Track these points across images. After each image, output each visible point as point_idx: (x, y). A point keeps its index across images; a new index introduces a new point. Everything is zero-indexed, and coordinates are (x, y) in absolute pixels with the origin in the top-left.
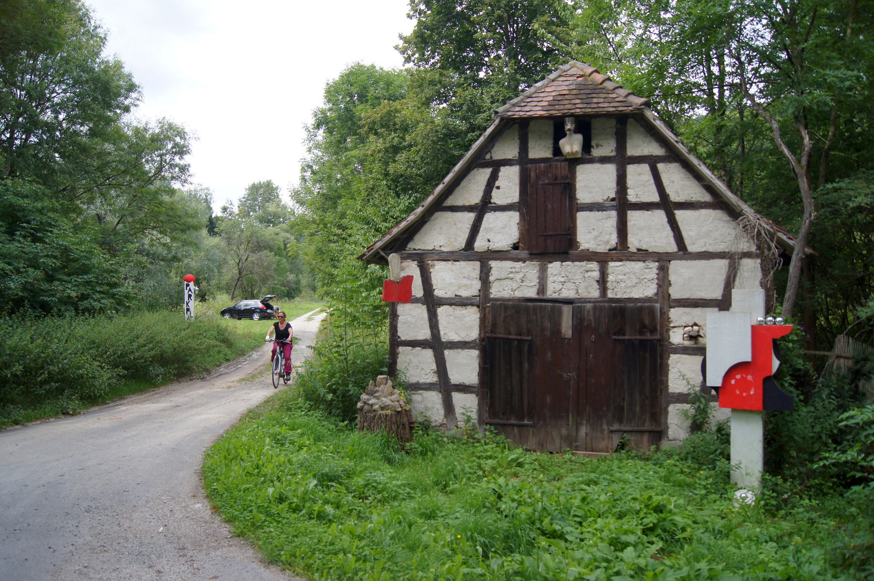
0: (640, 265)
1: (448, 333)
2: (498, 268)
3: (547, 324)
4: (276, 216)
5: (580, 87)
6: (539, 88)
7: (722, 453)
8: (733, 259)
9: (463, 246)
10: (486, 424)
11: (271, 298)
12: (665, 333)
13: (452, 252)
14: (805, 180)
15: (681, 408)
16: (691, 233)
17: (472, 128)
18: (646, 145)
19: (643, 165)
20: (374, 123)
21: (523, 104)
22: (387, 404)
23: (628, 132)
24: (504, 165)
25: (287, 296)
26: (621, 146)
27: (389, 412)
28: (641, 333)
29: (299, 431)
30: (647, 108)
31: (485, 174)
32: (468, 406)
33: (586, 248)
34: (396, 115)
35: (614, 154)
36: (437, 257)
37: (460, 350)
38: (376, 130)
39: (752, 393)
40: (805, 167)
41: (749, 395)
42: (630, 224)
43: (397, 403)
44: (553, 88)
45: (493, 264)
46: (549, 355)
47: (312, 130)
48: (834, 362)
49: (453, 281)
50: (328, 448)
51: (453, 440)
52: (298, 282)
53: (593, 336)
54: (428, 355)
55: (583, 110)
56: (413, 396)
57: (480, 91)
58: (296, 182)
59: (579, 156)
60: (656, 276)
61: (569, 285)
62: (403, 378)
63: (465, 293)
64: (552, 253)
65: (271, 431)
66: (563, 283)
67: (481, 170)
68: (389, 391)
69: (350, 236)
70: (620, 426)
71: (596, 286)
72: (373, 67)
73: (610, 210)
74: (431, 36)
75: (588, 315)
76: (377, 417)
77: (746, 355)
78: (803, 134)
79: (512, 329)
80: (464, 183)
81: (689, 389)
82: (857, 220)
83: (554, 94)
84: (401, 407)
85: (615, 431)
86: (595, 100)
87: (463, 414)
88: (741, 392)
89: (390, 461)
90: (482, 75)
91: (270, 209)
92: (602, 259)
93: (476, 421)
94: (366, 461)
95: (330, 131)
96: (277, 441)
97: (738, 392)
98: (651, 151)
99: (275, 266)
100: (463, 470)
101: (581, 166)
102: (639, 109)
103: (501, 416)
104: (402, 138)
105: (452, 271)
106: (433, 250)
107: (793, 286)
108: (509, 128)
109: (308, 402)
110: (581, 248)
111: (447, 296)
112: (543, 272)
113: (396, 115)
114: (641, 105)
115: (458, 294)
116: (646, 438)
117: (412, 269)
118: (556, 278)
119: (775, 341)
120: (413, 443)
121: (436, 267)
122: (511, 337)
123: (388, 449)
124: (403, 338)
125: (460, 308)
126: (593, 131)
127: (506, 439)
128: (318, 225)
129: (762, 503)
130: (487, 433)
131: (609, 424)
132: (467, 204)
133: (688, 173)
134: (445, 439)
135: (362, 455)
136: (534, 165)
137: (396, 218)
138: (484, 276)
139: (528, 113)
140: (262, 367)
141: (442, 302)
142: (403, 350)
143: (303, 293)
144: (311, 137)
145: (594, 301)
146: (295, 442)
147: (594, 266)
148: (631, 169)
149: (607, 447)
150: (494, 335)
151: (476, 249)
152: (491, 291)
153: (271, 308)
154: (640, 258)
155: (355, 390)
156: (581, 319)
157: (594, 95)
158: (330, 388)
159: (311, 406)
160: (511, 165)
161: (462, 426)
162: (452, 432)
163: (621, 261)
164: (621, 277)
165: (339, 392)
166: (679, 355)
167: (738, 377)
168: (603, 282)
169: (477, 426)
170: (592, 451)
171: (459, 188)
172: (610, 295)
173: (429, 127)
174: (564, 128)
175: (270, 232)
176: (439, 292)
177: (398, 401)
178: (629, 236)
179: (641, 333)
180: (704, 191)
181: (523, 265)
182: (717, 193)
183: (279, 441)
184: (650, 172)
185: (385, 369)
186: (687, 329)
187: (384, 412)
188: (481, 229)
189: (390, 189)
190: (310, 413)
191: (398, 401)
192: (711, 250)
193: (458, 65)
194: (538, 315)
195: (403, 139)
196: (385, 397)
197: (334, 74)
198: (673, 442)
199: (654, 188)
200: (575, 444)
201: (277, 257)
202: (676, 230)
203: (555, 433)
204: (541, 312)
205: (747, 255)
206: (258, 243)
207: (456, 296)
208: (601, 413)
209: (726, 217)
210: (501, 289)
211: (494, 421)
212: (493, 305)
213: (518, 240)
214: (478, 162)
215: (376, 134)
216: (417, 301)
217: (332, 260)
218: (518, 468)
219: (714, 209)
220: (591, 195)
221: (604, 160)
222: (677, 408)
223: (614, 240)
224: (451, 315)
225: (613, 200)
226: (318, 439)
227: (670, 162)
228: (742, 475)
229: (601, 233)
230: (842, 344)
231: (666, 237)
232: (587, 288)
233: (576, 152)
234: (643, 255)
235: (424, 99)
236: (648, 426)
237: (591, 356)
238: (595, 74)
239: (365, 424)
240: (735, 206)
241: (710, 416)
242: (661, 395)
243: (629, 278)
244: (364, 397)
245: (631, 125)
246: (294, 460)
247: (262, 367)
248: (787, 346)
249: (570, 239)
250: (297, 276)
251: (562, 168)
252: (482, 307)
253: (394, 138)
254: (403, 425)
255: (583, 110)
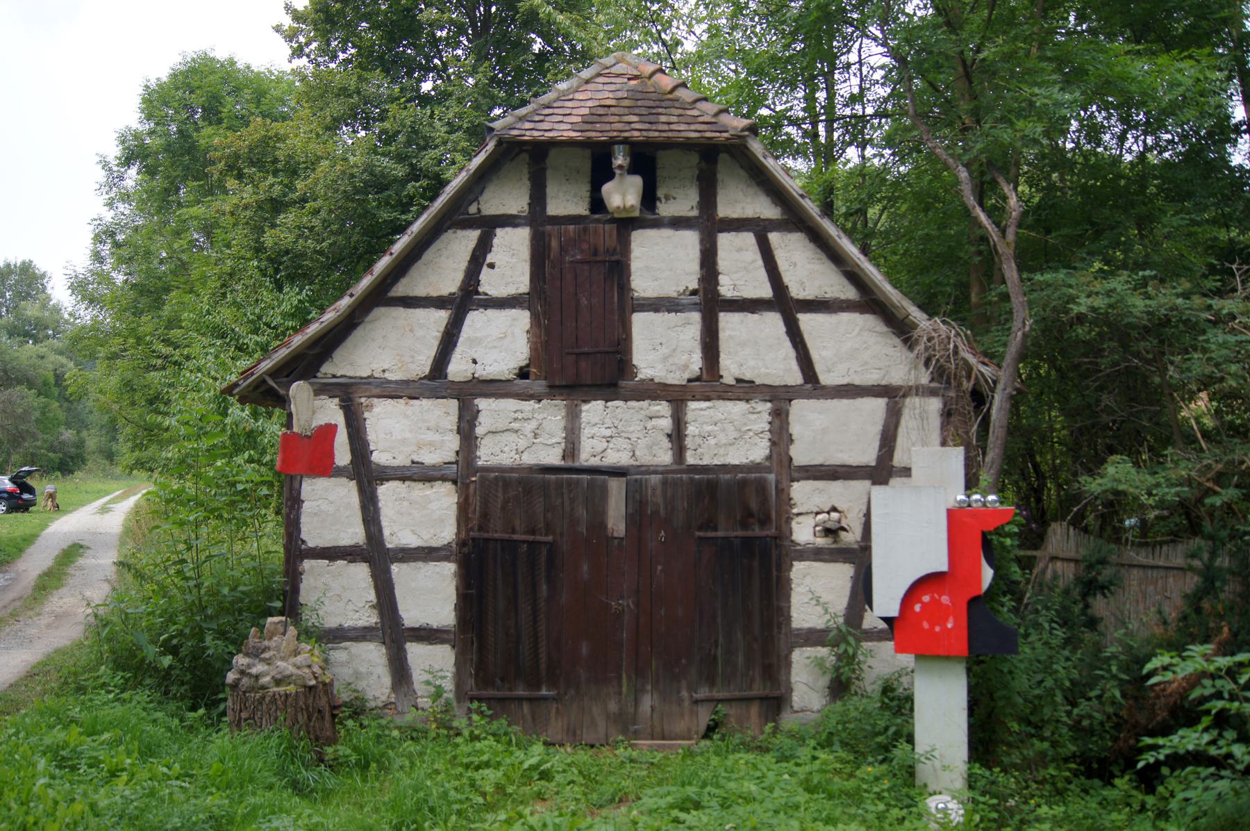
0: (741, 407)
1: (397, 533)
2: (490, 410)
3: (582, 512)
4: (41, 325)
5: (636, 95)
6: (565, 93)
7: (898, 735)
8: (892, 395)
9: (427, 370)
10: (472, 700)
11: (29, 473)
12: (784, 525)
13: (406, 383)
14: (1013, 265)
15: (813, 655)
16: (824, 353)
17: (415, 174)
18: (749, 200)
19: (745, 234)
20: (237, 156)
21: (537, 118)
22: (288, 673)
23: (719, 177)
24: (503, 226)
25: (59, 469)
26: (708, 200)
27: (291, 689)
28: (745, 525)
29: (106, 736)
30: (753, 136)
31: (466, 240)
32: (437, 667)
33: (649, 376)
34: (278, 145)
35: (695, 213)
36: (377, 391)
37: (420, 564)
38: (240, 170)
39: (950, 626)
40: (1013, 245)
41: (945, 629)
42: (723, 335)
43: (307, 670)
44: (588, 95)
45: (482, 404)
46: (585, 568)
47: (115, 169)
48: (1047, 567)
49: (408, 435)
50: (169, 768)
51: (414, 733)
52: (80, 444)
53: (663, 533)
54: (361, 573)
55: (645, 134)
56: (332, 652)
57: (429, 112)
58: (82, 262)
59: (637, 214)
60: (767, 427)
61: (620, 442)
62: (314, 620)
63: (430, 458)
64: (588, 386)
65: (48, 741)
66: (609, 439)
67: (460, 233)
68: (292, 648)
69: (188, 358)
70: (711, 691)
71: (666, 444)
72: (232, 63)
73: (690, 310)
74: (341, 13)
75: (654, 494)
76: (267, 699)
77: (939, 562)
78: (1006, 190)
79: (517, 523)
80: (428, 255)
81: (829, 621)
82: (1077, 336)
83: (590, 104)
84: (316, 678)
85: (702, 701)
86: (663, 119)
87: (428, 683)
88: (932, 625)
89: (298, 788)
90: (426, 87)
91: (29, 313)
92: (677, 396)
93: (451, 696)
94: (254, 794)
95: (150, 171)
96: (62, 763)
97: (926, 625)
98: (758, 210)
99: (37, 414)
100: (445, 794)
101: (640, 231)
102: (740, 137)
103: (498, 681)
104: (286, 186)
105: (406, 416)
106: (369, 377)
107: (999, 442)
108: (512, 160)
109: (121, 674)
110: (640, 376)
111: (396, 463)
112: (573, 418)
113: (278, 145)
114: (743, 130)
115: (416, 459)
116: (754, 710)
117: (330, 412)
118: (595, 430)
119: (984, 535)
120: (339, 747)
121: (376, 410)
122: (515, 537)
123: (293, 763)
124: (311, 544)
125: (420, 485)
126: (659, 173)
127: (509, 725)
128: (126, 338)
129: (977, 818)
130: (475, 717)
131: (692, 689)
132: (434, 294)
133: (819, 251)
134: (396, 733)
135: (237, 784)
136: (556, 227)
137: (274, 328)
138: (465, 425)
139: (547, 134)
140: (18, 603)
141: (387, 474)
142: (312, 567)
143: (90, 464)
144: (114, 179)
145: (664, 471)
146: (100, 762)
147: (663, 408)
148: (725, 241)
149: (689, 730)
150: (486, 535)
151: (450, 378)
152: (478, 454)
153: (31, 490)
154: (742, 396)
155: (216, 647)
156: (641, 502)
157: (660, 110)
158: (165, 644)
159: (127, 680)
160: (515, 226)
161: (426, 706)
162: (408, 718)
163: (708, 399)
164: (710, 428)
165: (183, 652)
166: (807, 563)
167: (926, 599)
168: (677, 437)
169: (455, 704)
170: (663, 739)
171: (419, 264)
172: (691, 459)
173: (338, 167)
174: (611, 163)
175: (29, 354)
176: (380, 457)
177: (309, 666)
178: (723, 357)
179: (745, 525)
180: (845, 282)
181: (537, 406)
182: (867, 285)
183: (65, 761)
184: (757, 247)
185: (278, 604)
186: (820, 517)
187: (281, 689)
188: (461, 340)
189: (265, 275)
190: (125, 695)
191: (309, 666)
192: (857, 382)
193: (390, 65)
194: (566, 497)
195: (291, 187)
196: (282, 659)
197: (160, 70)
198: (801, 715)
199: (762, 274)
200: (632, 728)
201: (42, 399)
202: (800, 346)
203: (596, 711)
204: (570, 491)
205: (918, 390)
206: (5, 371)
207: (413, 462)
208: (677, 670)
209: (880, 327)
210: (497, 450)
211: (484, 693)
212: (483, 479)
213: (527, 362)
214: (454, 218)
215: (240, 176)
216: (339, 472)
217: (151, 402)
218: (543, 782)
219: (862, 313)
220: (656, 283)
221: (678, 223)
222: (807, 654)
223: (696, 363)
224: (403, 499)
225: (694, 293)
226: (148, 751)
227: (790, 231)
228: (935, 770)
229: (674, 350)
230: (1058, 537)
231: (785, 359)
232: (650, 447)
233: (632, 206)
234: (745, 390)
235: (329, 119)
236: (758, 690)
237: (659, 568)
238: (659, 75)
239: (244, 715)
240: (896, 307)
241: (865, 667)
242: (780, 633)
243: (723, 430)
244: (240, 660)
245: (724, 163)
246: (103, 803)
247: (18, 603)
248: (1002, 544)
249: (621, 361)
250: (78, 432)
251: (607, 235)
252: (462, 483)
253: (272, 185)
254: (320, 711)
255: (645, 134)
